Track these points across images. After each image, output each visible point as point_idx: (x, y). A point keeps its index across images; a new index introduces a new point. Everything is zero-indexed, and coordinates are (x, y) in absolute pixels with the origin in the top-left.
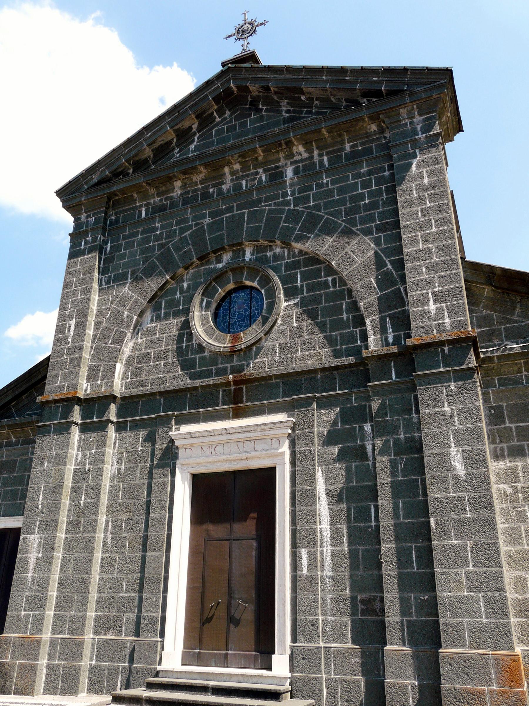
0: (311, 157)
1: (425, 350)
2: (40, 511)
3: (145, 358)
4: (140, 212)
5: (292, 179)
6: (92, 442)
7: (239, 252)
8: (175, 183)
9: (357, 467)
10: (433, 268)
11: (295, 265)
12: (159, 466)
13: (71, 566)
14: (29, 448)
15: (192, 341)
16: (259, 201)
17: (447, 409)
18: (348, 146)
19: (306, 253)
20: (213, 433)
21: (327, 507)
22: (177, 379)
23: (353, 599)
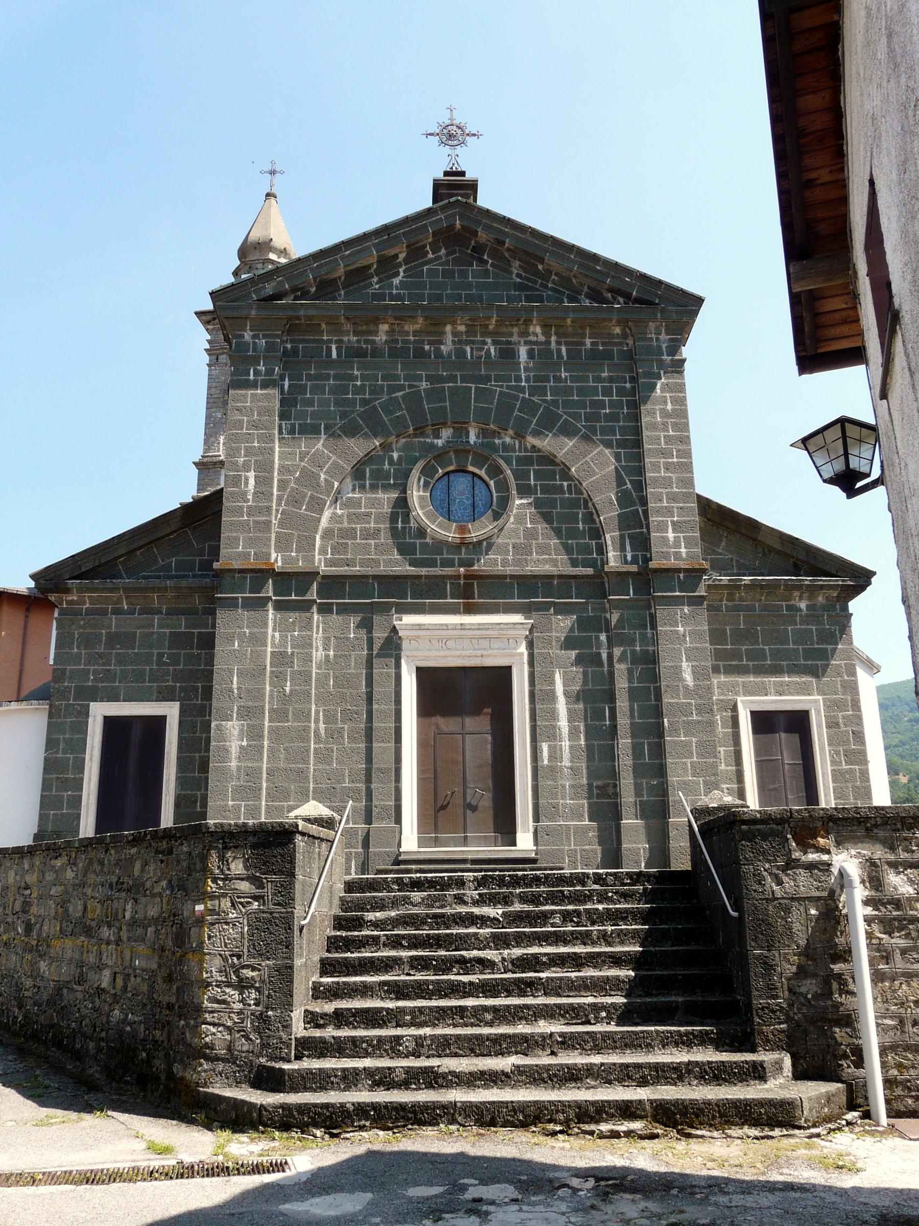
0: (548, 343)
1: (663, 574)
2: (236, 696)
3: (349, 533)
4: (329, 350)
5: (527, 363)
6: (293, 623)
7: (461, 431)
8: (380, 326)
9: (593, 672)
10: (672, 498)
11: (527, 461)
12: (379, 656)
13: (282, 756)
14: (154, 620)
15: (409, 522)
16: (488, 379)
17: (681, 629)
18: (588, 341)
19: (539, 450)
20: (446, 627)
21: (565, 706)
22: (395, 564)
23: (590, 785)
